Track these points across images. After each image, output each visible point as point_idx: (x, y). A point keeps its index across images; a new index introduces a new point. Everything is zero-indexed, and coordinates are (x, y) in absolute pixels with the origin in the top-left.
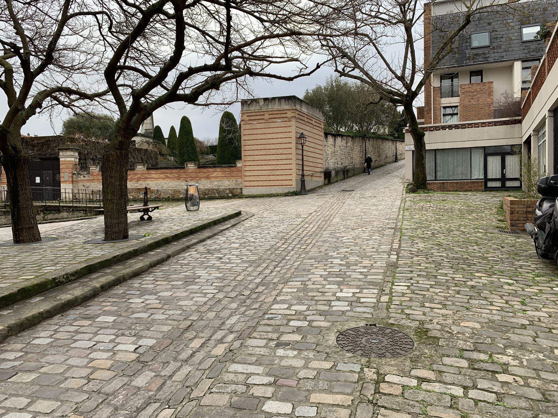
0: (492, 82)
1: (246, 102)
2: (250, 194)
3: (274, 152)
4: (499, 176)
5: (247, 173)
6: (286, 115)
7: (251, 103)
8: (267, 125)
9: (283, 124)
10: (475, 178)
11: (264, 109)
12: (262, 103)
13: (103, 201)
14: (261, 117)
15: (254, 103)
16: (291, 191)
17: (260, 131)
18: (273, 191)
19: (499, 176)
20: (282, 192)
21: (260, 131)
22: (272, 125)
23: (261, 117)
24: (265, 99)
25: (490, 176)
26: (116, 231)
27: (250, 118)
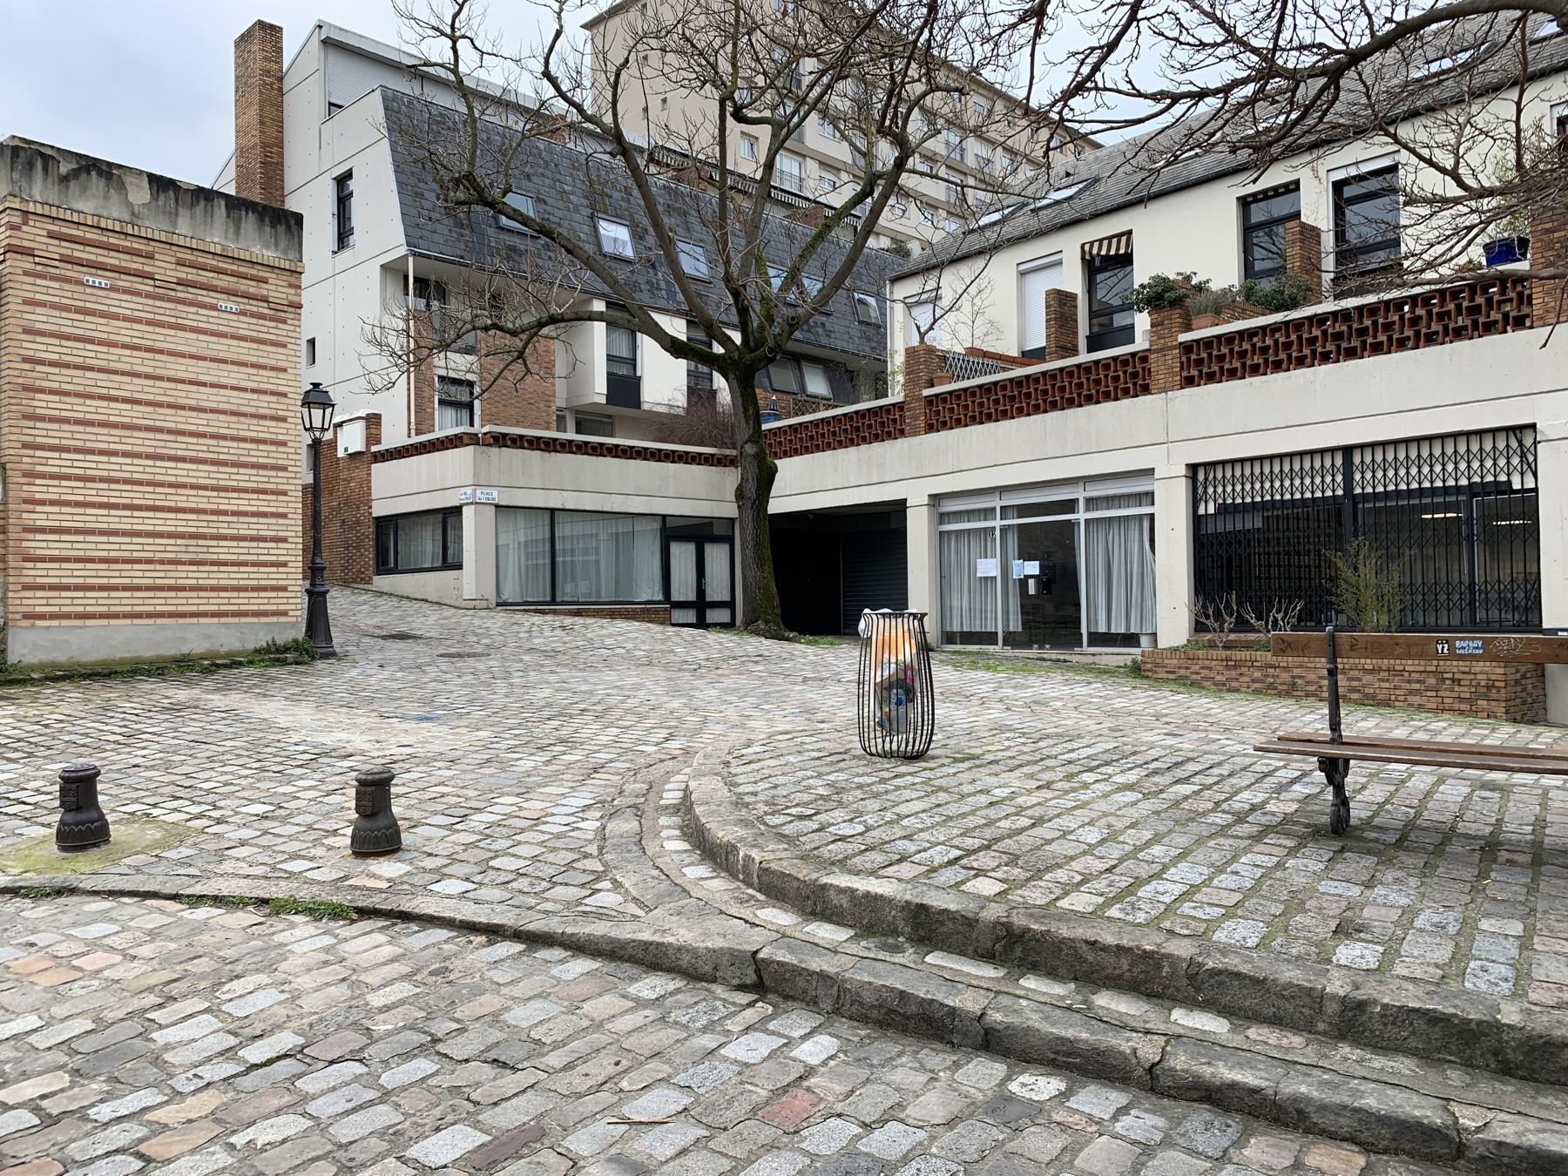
0: (1293, 187)
1: (46, 159)
2: (61, 657)
3: (200, 447)
4: (691, 596)
5: (39, 545)
6: (263, 290)
7: (75, 174)
8: (165, 311)
9: (245, 326)
10: (644, 598)
11: (154, 226)
12: (140, 195)
13: (1470, 485)
14: (136, 264)
15: (96, 182)
16: (280, 641)
17: (125, 332)
18: (195, 639)
19: (691, 596)
20: (236, 646)
21: (125, 332)
22: (193, 317)
23: (136, 264)
24: (161, 185)
25: (675, 597)
26: (1107, 263)
27: (66, 249)
